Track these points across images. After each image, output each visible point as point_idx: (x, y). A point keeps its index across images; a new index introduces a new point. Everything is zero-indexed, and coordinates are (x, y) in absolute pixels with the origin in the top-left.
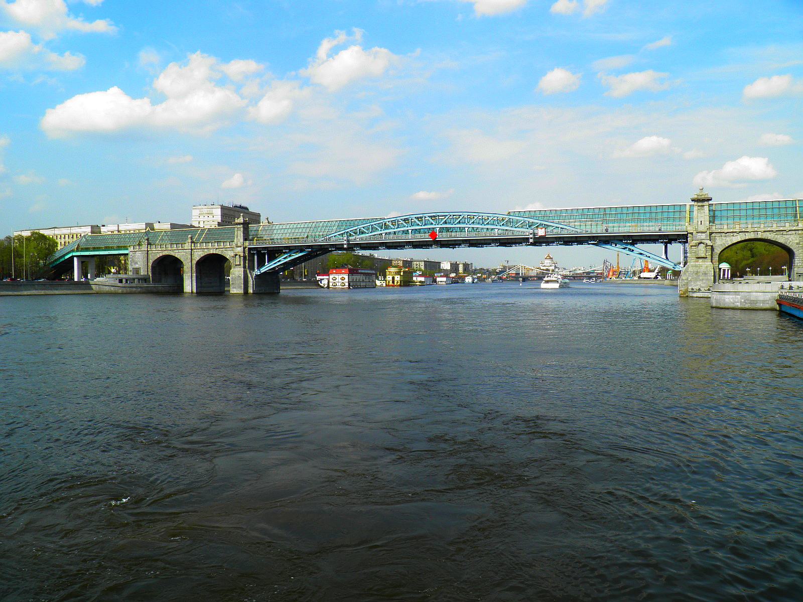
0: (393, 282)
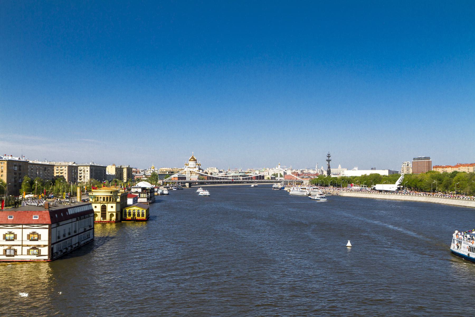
0: (104, 215)
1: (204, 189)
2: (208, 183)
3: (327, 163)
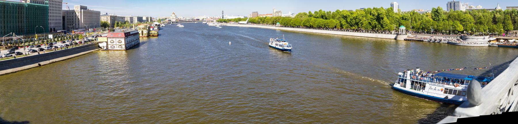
1: (181, 24)
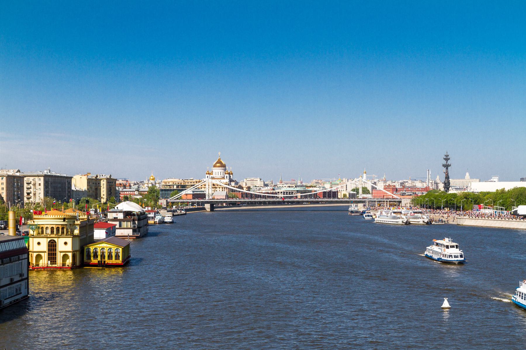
0: (52, 257)
2: (243, 203)
3: (444, 169)
